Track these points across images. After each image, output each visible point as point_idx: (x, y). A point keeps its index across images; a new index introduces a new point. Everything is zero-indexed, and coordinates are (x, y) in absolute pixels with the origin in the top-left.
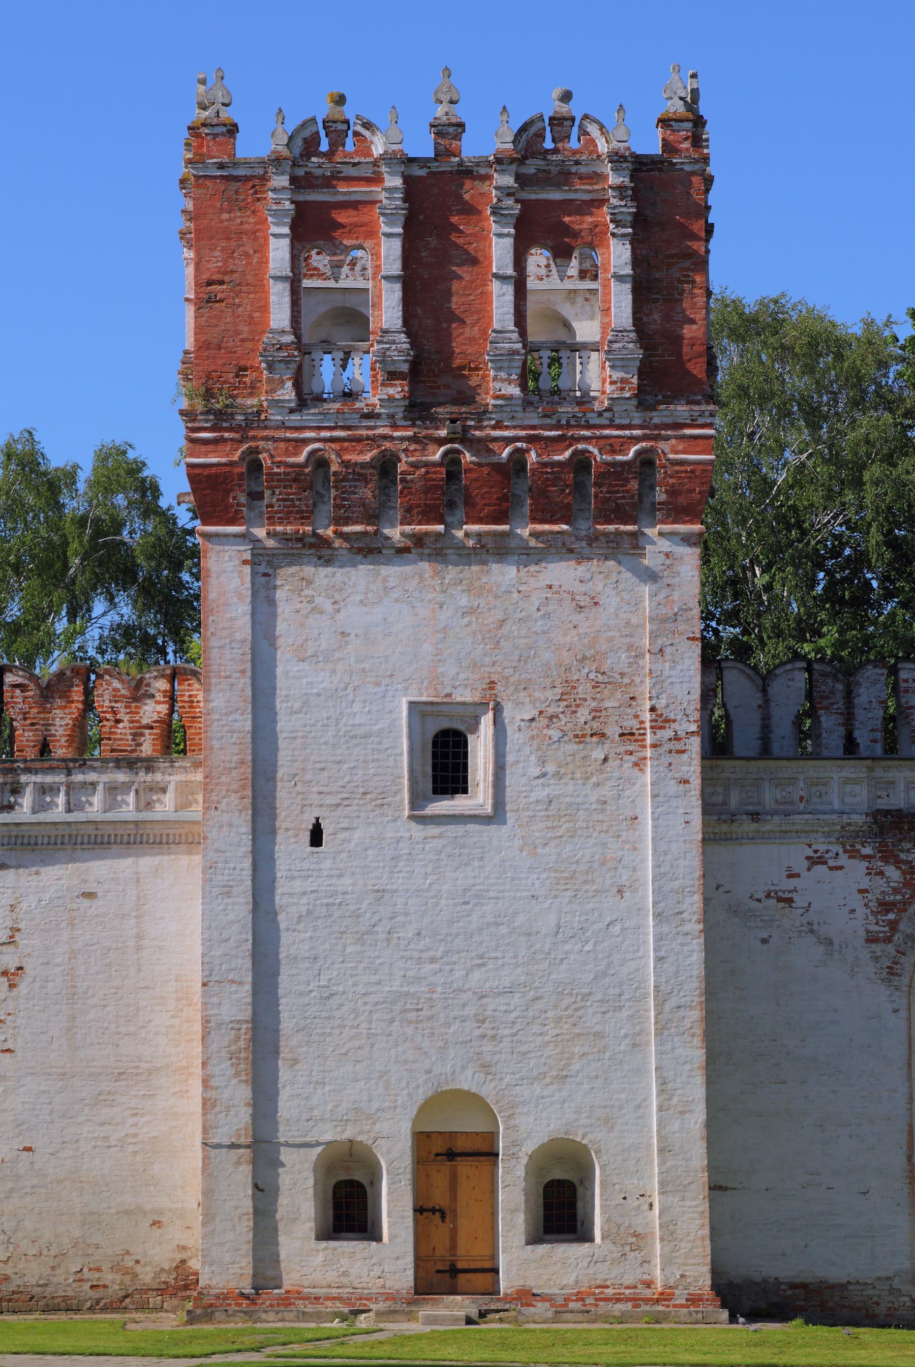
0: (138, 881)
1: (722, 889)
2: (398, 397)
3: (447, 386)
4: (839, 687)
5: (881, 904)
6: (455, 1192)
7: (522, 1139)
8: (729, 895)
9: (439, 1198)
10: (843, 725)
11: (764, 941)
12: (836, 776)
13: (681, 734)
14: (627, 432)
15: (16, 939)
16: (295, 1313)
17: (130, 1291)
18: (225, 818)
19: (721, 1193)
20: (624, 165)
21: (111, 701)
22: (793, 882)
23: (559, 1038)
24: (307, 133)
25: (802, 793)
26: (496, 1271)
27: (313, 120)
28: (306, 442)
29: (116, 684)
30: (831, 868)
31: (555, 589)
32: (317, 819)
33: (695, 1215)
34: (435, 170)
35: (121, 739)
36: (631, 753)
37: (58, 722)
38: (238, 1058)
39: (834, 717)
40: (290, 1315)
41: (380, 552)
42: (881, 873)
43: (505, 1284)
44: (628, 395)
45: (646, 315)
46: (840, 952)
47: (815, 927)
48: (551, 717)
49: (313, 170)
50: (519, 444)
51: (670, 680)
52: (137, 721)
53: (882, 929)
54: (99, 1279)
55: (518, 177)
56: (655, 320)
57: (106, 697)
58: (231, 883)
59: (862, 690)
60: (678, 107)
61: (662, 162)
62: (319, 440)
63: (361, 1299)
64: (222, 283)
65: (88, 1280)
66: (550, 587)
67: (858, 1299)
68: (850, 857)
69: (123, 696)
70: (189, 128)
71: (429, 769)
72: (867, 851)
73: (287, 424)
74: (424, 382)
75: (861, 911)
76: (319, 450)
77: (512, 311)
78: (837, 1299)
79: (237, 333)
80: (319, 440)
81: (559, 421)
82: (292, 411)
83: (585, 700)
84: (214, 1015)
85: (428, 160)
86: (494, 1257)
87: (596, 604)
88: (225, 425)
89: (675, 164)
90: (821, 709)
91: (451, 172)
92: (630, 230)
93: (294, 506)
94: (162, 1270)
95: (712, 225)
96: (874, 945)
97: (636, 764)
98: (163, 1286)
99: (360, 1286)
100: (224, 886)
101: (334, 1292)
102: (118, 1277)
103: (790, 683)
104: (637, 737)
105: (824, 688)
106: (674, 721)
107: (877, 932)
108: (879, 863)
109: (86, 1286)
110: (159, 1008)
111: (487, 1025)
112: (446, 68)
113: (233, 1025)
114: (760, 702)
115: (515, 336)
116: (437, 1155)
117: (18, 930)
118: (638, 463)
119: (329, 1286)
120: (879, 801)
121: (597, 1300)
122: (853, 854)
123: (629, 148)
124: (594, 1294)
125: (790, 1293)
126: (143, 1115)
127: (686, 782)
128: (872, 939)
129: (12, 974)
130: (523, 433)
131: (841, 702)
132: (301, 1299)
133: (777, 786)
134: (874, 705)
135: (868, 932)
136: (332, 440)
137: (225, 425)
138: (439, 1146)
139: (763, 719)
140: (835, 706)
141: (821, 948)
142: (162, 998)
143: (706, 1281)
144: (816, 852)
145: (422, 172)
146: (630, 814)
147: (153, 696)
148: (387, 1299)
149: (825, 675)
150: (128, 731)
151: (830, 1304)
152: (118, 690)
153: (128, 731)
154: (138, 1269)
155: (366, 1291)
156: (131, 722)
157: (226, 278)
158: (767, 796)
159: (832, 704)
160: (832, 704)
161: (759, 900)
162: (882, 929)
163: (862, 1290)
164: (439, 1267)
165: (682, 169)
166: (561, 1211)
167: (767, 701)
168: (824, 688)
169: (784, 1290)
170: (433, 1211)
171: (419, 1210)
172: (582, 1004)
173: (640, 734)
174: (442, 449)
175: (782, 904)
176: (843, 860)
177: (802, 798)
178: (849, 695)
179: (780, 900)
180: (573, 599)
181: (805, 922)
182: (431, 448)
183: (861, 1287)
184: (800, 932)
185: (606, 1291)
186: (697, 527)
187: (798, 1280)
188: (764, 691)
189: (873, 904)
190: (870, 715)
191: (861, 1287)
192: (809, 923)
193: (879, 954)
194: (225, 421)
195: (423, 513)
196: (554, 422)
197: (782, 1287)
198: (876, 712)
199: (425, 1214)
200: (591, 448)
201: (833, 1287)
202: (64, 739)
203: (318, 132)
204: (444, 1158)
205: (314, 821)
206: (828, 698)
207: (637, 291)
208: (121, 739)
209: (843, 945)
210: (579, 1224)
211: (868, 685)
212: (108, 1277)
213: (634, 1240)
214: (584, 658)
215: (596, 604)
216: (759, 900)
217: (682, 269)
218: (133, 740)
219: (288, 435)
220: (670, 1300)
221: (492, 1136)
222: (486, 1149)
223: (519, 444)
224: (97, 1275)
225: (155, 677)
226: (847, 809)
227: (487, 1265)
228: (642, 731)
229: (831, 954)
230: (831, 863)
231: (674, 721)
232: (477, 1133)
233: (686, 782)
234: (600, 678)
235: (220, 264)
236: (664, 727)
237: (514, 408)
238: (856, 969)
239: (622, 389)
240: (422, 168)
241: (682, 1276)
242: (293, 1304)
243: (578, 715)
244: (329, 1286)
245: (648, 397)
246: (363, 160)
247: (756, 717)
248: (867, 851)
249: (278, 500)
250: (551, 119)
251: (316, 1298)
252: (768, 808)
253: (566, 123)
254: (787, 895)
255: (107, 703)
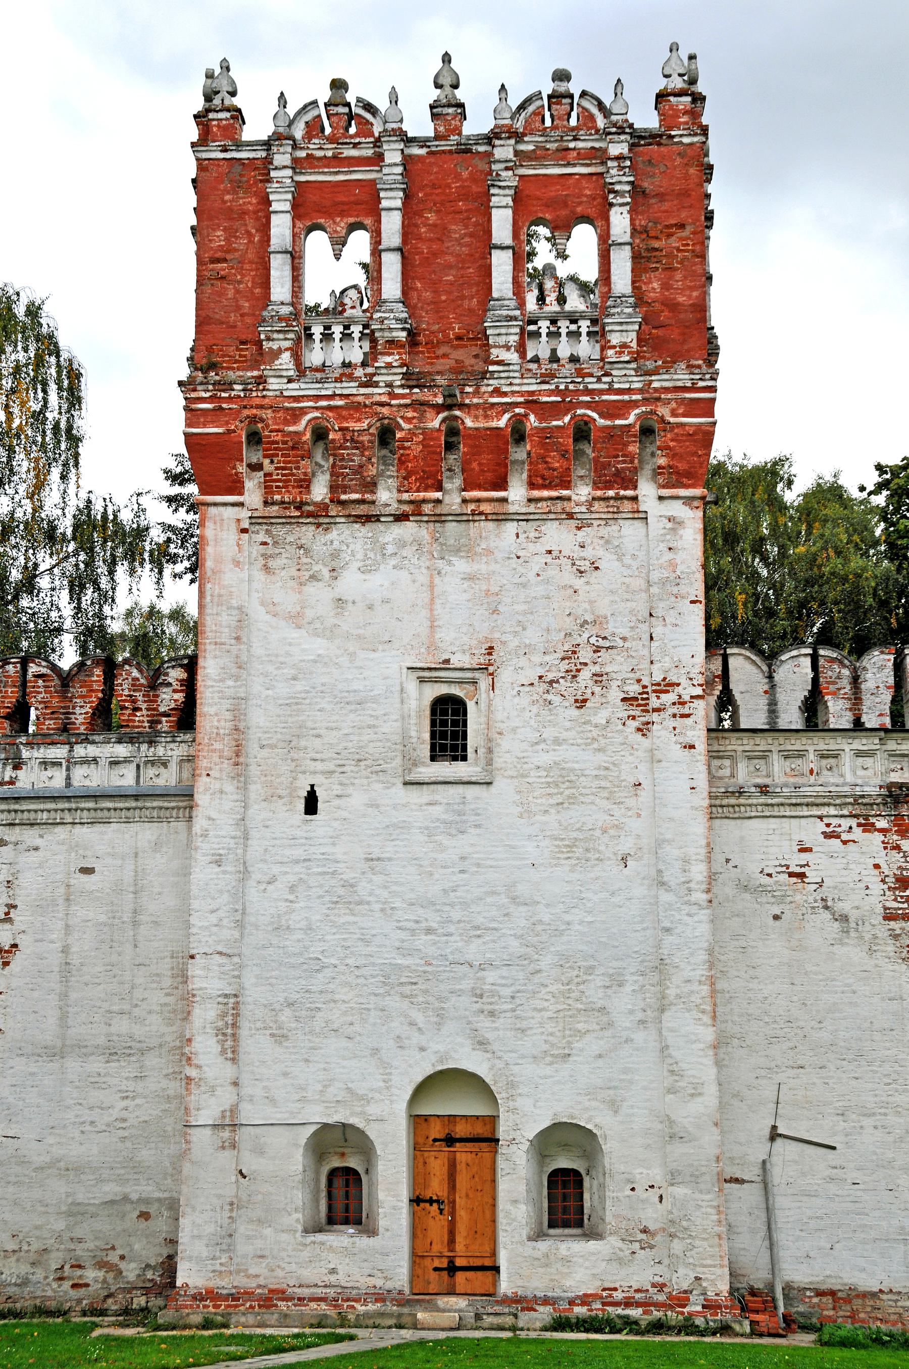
0: (136, 855)
1: (731, 864)
2: (395, 364)
3: (445, 356)
4: (846, 672)
5: (898, 879)
6: (454, 1181)
7: (521, 1123)
8: (738, 870)
9: (437, 1188)
10: (851, 709)
11: (776, 917)
12: (847, 748)
13: (686, 698)
14: (626, 397)
15: (12, 915)
16: (276, 1316)
17: (113, 1290)
18: (217, 785)
19: (738, 1186)
20: (623, 137)
21: (130, 690)
22: (805, 856)
23: (561, 1014)
24: (309, 117)
25: (812, 765)
26: (496, 1269)
27: (314, 103)
28: (303, 411)
29: (135, 673)
30: (845, 842)
31: (554, 554)
32: (312, 786)
33: (709, 1210)
34: (434, 149)
35: (138, 727)
36: (634, 718)
37: (78, 710)
38: (224, 1034)
39: (841, 702)
40: (273, 1318)
41: (378, 520)
42: (898, 848)
43: (505, 1286)
44: (627, 358)
45: (645, 283)
46: (857, 930)
47: (829, 904)
48: (551, 682)
49: (314, 152)
50: (517, 410)
51: (673, 644)
52: (154, 709)
53: (901, 906)
54: (80, 1277)
55: (517, 153)
56: (654, 289)
57: (125, 686)
58: (221, 852)
59: (869, 676)
60: (678, 83)
61: (661, 136)
62: (317, 408)
63: (348, 1300)
64: (225, 260)
65: (69, 1278)
66: (550, 552)
67: (892, 1310)
68: (864, 831)
69: (142, 685)
70: (195, 117)
71: (427, 736)
72: (882, 824)
73: (286, 393)
74: (423, 353)
75: (877, 888)
76: (316, 418)
77: (511, 280)
78: (869, 1309)
79: (238, 308)
80: (317, 408)
81: (557, 387)
82: (290, 381)
83: (586, 664)
84: (201, 989)
85: (427, 139)
86: (494, 1254)
87: (597, 568)
88: (223, 395)
89: (674, 137)
90: (828, 694)
91: (450, 151)
92: (629, 200)
93: (293, 475)
94: (148, 1266)
95: (712, 212)
96: (892, 923)
97: (639, 730)
98: (149, 1285)
99: (349, 1285)
100: (213, 855)
101: (319, 1292)
102: (101, 1274)
103: (796, 669)
104: (640, 702)
105: (830, 673)
106: (678, 685)
107: (895, 909)
108: (895, 837)
109: (67, 1285)
110: (155, 985)
111: (485, 1000)
112: (446, 54)
113: (220, 999)
114: (766, 687)
115: (513, 304)
116: (435, 1140)
117: (15, 907)
118: (638, 427)
119: (316, 1285)
120: (892, 774)
121: (604, 1304)
122: (868, 827)
123: (627, 121)
124: (602, 1297)
125: (815, 1300)
126: (134, 1098)
127: (692, 747)
128: (890, 916)
129: (6, 952)
130: (521, 399)
131: (848, 687)
132: (283, 1300)
133: (786, 757)
134: (882, 690)
135: (886, 908)
136: (330, 408)
137: (223, 395)
138: (436, 1131)
139: (769, 705)
140: (842, 692)
141: (836, 925)
142: (158, 975)
143: (724, 1287)
144: (828, 825)
145: (423, 152)
146: (632, 780)
147: (170, 684)
148: (377, 1301)
149: (832, 660)
150: (146, 719)
151: (862, 1315)
152: (138, 679)
153: (146, 719)
154: (123, 1265)
155: (354, 1292)
156: (148, 709)
157: (228, 257)
158: (776, 769)
159: (839, 689)
160: (839, 689)
161: (770, 875)
162: (901, 906)
163: (896, 1301)
164: (437, 1264)
165: (681, 143)
166: (566, 1202)
167: (773, 687)
168: (830, 673)
169: (810, 1297)
170: (431, 1201)
171: (416, 1201)
172: (585, 977)
173: (643, 699)
174: (441, 416)
175: (794, 880)
176: (857, 834)
177: (811, 772)
178: (856, 680)
179: (791, 875)
180: (574, 564)
181: (818, 898)
182: (430, 413)
183: (895, 1297)
184: (813, 908)
185: (615, 1294)
186: (698, 492)
187: (823, 1287)
188: (770, 677)
189: (890, 880)
190: (878, 700)
191: (895, 1297)
192: (822, 899)
193: (898, 932)
194: (224, 391)
195: (421, 480)
196: (553, 387)
197: (808, 1293)
198: (883, 696)
199: (422, 1205)
200: (589, 413)
201: (864, 1295)
202: (83, 728)
203: (319, 116)
204: (443, 1143)
205: (309, 789)
206: (834, 683)
207: (636, 257)
208: (138, 727)
209: (860, 923)
210: (586, 1217)
211: (875, 670)
212: (91, 1274)
213: (644, 1236)
214: (586, 622)
215: (597, 568)
216: (770, 875)
217: (681, 239)
218: (150, 727)
219: (286, 404)
220: (684, 1306)
221: (493, 1120)
222: (487, 1135)
223: (517, 410)
224: (79, 1272)
225: (173, 667)
226: (859, 782)
227: (488, 1263)
228: (645, 696)
229: (848, 932)
230: (845, 837)
231: (678, 685)
232: (477, 1117)
233: (692, 747)
234: (601, 643)
235: (223, 243)
236: (667, 692)
237: (512, 374)
238: (875, 948)
239: (621, 353)
240: (422, 147)
241: (697, 1279)
242: (276, 1306)
243: (579, 679)
244: (316, 1285)
245: (648, 363)
246: (363, 140)
247: (763, 702)
248: (882, 824)
249: (277, 468)
250: (550, 97)
251: (299, 1299)
252: (777, 781)
253: (564, 101)
254: (798, 870)
255: (126, 692)
